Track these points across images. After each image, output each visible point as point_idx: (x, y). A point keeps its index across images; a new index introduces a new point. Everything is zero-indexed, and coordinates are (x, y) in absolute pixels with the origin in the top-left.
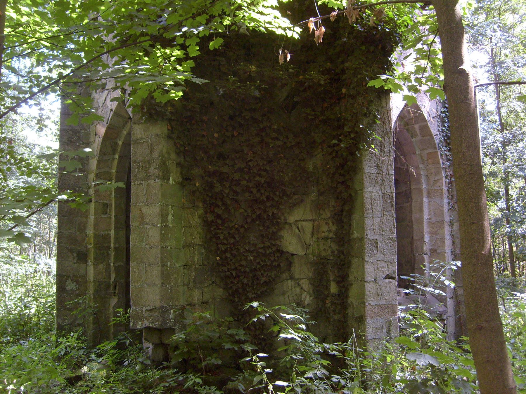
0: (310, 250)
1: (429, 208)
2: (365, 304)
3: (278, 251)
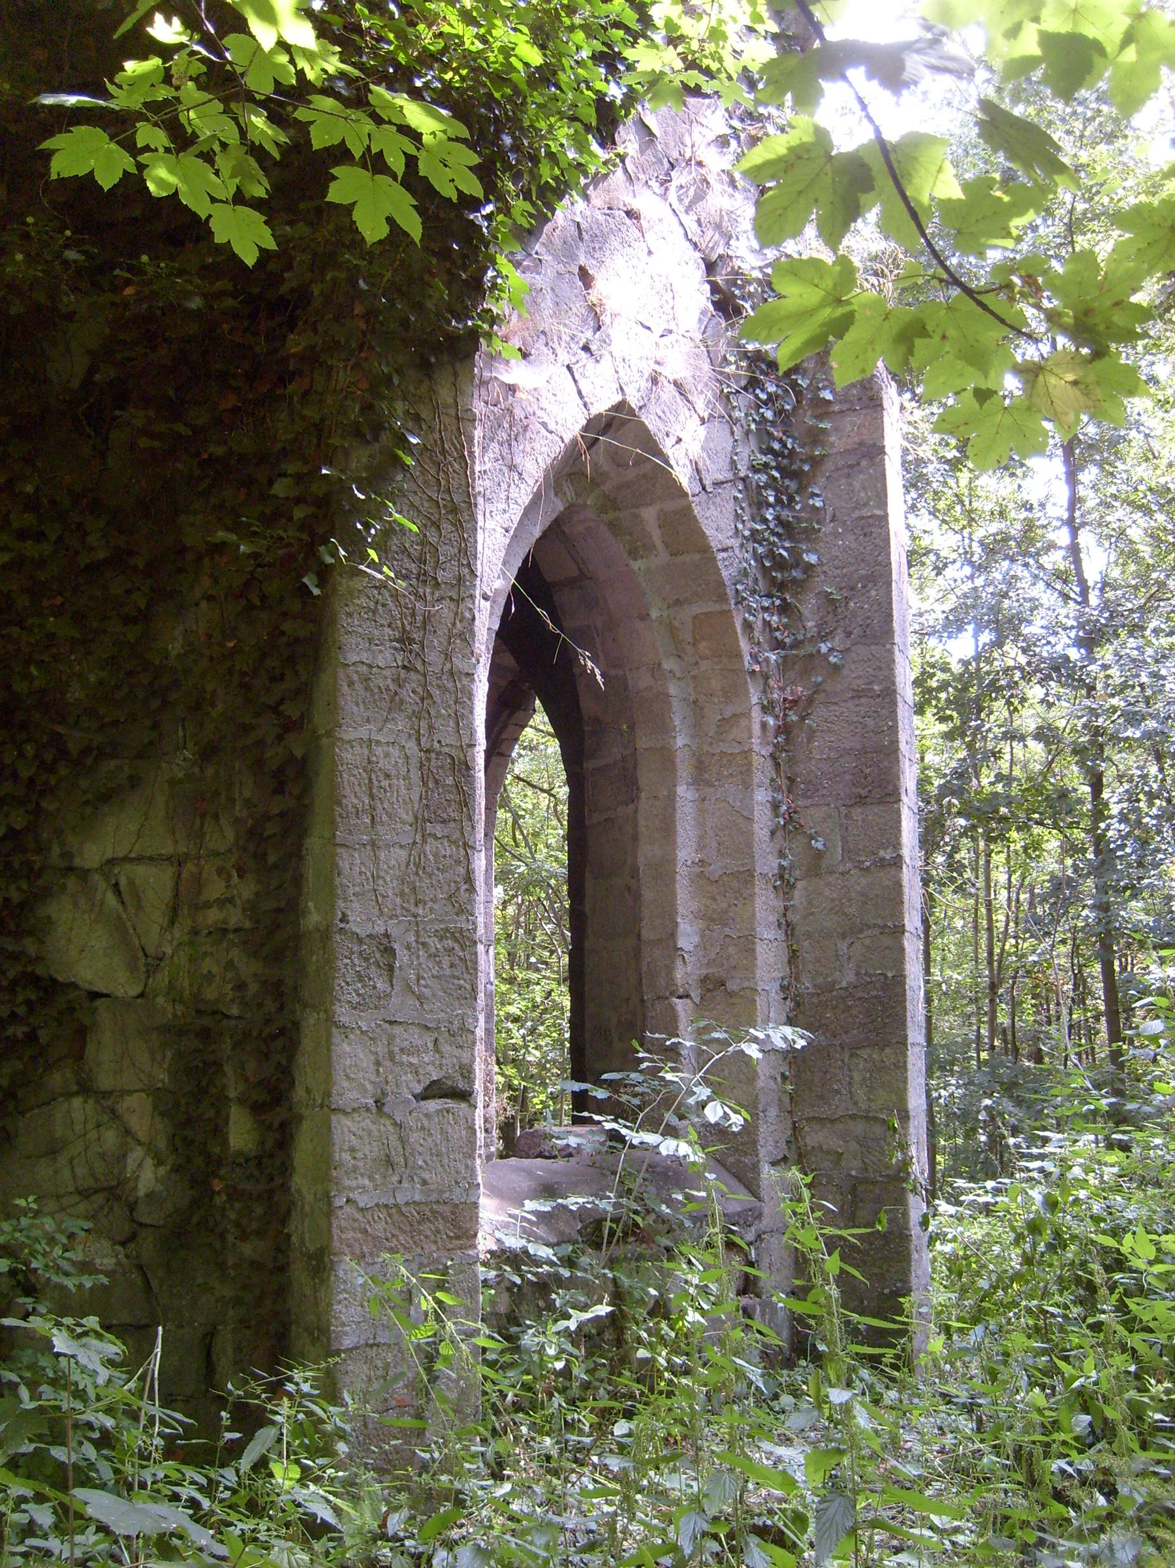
0: (162, 979)
1: (701, 825)
2: (330, 1204)
3: (35, 980)
